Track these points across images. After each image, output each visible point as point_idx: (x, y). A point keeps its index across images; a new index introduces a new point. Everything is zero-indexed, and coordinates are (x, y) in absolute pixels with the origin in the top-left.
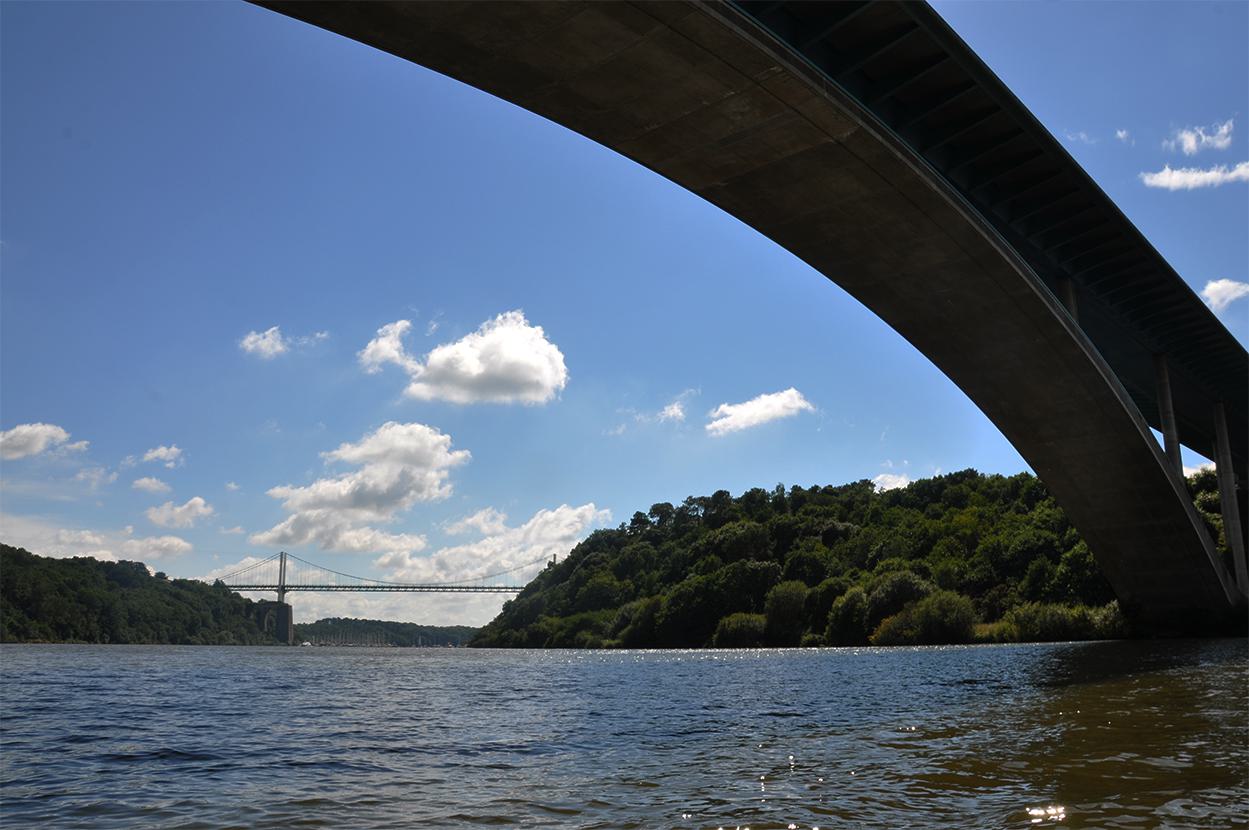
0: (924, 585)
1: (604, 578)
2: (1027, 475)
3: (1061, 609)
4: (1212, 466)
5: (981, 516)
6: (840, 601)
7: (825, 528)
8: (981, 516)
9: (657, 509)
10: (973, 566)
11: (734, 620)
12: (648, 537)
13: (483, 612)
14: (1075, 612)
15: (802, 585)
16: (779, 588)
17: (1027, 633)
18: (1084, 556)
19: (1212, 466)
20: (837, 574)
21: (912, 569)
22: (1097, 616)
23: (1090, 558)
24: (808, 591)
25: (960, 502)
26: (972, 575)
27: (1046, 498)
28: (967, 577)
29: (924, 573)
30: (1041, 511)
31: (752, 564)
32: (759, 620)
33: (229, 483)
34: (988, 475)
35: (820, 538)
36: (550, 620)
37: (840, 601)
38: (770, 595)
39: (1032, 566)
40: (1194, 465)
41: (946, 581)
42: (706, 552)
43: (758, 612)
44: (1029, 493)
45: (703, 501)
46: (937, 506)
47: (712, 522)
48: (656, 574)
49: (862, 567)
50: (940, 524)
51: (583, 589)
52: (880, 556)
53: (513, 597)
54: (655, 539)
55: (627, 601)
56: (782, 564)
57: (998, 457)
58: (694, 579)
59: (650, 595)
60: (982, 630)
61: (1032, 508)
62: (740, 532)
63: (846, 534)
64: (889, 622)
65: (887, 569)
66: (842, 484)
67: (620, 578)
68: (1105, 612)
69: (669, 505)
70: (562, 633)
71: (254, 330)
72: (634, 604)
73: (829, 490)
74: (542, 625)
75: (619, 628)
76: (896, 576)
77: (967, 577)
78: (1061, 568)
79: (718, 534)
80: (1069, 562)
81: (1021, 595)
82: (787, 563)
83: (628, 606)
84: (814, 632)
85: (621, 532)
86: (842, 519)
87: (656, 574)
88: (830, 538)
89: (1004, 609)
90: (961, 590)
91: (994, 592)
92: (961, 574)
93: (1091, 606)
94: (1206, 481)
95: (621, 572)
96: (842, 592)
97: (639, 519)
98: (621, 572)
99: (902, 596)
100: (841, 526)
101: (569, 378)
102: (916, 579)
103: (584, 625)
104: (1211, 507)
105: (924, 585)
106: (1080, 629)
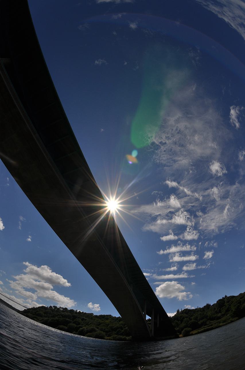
0: (97, 330)
1: (41, 313)
2: (120, 317)
3: (121, 336)
4: (150, 318)
5: (110, 322)
6: (81, 329)
7: (82, 318)
8: (110, 322)
9: (54, 307)
10: (107, 328)
11: (61, 326)
12: (51, 310)
13: (22, 309)
14: (124, 337)
15: (75, 325)
16: (70, 324)
17: (114, 339)
18: (127, 329)
19: (150, 318)
20: (82, 325)
21: (95, 327)
22: (127, 338)
23: (128, 330)
24: (76, 326)
25: (107, 319)
26: (106, 330)
27: (122, 321)
28: (105, 330)
29: (98, 328)
30: (121, 322)
31: (67, 319)
32: (66, 328)
33: (159, 251)
34: (113, 316)
35: (81, 319)
36: (31, 315)
37: (81, 329)
38: (69, 324)
39: (118, 330)
40: (148, 317)
41: (101, 330)
42: (60, 315)
43: (66, 326)
44: (120, 319)
45: (62, 308)
46: (103, 319)
47: (63, 311)
48: (50, 315)
49: (87, 325)
50: (103, 322)
51: (37, 313)
52: (91, 324)
53: (26, 309)
54: (53, 310)
55: (44, 317)
56: (73, 321)
57: (116, 314)
58: (56, 318)
59: (48, 318)
60: (106, 338)
61: (120, 322)
62: (67, 314)
63: (86, 320)
64: (89, 334)
65: (91, 326)
66: (88, 313)
67: (45, 314)
68: (129, 337)
69: (57, 307)
70: (32, 317)
71: (28, 262)
72: (45, 318)
73: (85, 313)
74: (29, 315)
75: (41, 320)
76: (92, 327)
77: (105, 330)
78: (123, 331)
79: (63, 313)
80: (124, 330)
81: (115, 334)
82: (74, 321)
83: (44, 318)
84: (76, 332)
85: (47, 308)
86: (86, 317)
87: (50, 315)
88: (83, 319)
89: (111, 335)
90: (104, 332)
91: (110, 333)
92: (104, 329)
93: (127, 336)
94: (149, 320)
95: (45, 313)
96: (82, 327)
97: (51, 307)
98: (45, 313)
99: (92, 330)
100: (85, 318)
101: (31, 292)
102: (96, 328)
103: (35, 317)
104: (150, 324)
105: (97, 330)
106: (125, 339)
